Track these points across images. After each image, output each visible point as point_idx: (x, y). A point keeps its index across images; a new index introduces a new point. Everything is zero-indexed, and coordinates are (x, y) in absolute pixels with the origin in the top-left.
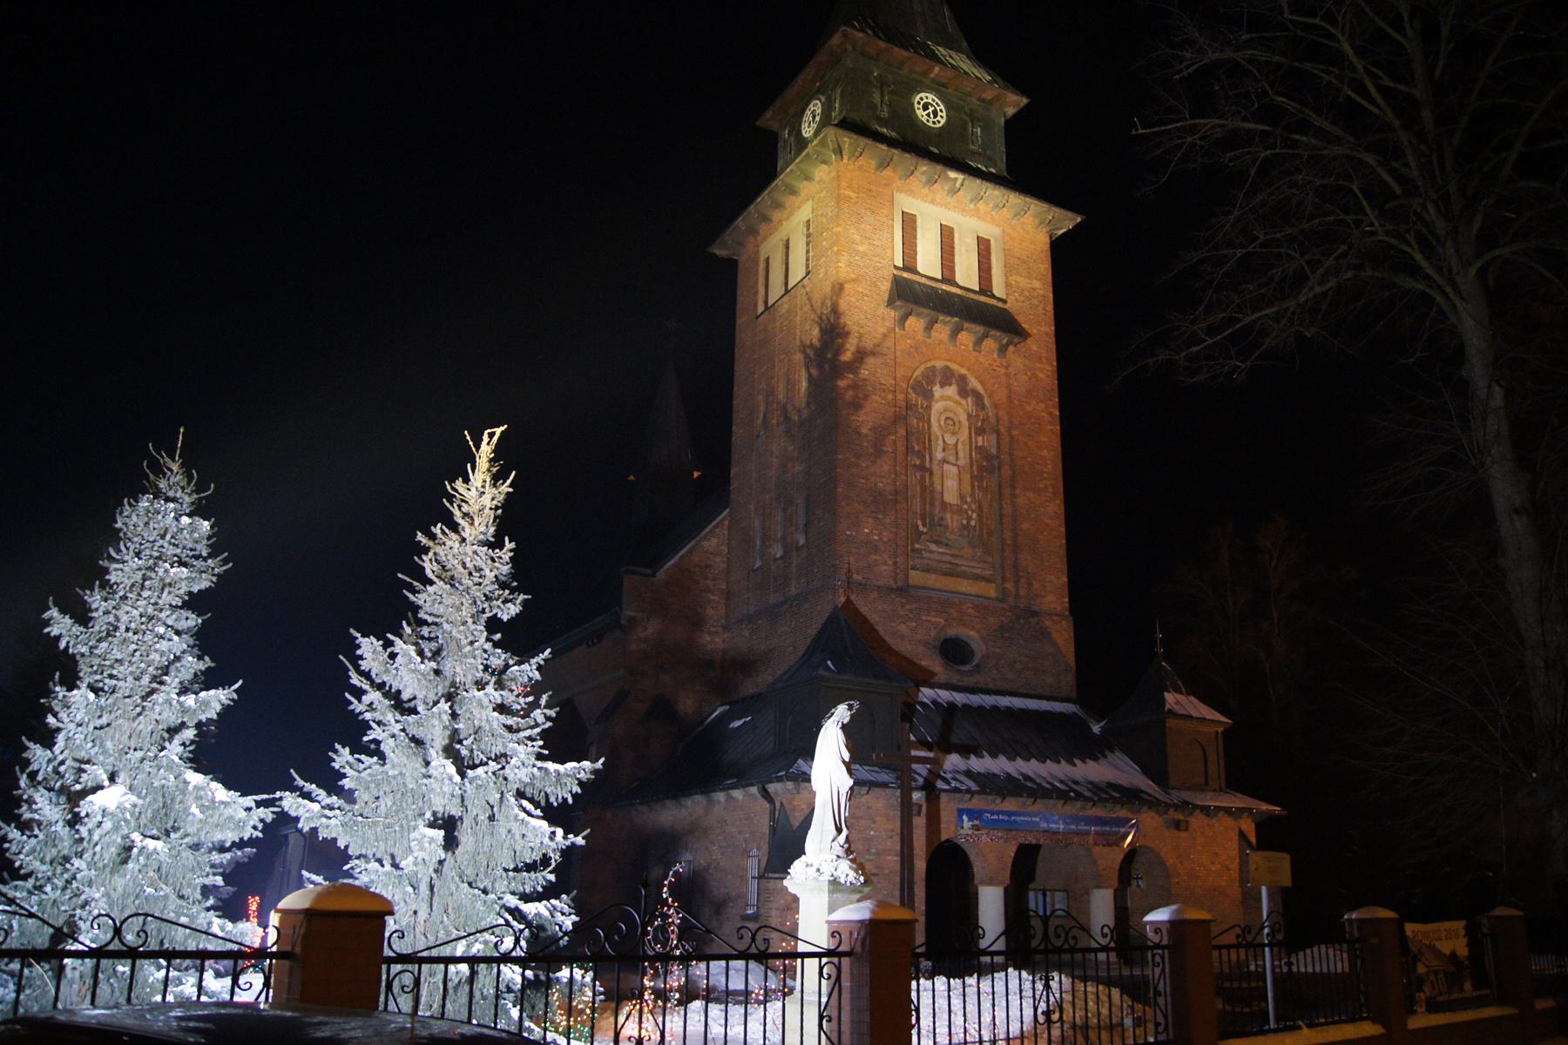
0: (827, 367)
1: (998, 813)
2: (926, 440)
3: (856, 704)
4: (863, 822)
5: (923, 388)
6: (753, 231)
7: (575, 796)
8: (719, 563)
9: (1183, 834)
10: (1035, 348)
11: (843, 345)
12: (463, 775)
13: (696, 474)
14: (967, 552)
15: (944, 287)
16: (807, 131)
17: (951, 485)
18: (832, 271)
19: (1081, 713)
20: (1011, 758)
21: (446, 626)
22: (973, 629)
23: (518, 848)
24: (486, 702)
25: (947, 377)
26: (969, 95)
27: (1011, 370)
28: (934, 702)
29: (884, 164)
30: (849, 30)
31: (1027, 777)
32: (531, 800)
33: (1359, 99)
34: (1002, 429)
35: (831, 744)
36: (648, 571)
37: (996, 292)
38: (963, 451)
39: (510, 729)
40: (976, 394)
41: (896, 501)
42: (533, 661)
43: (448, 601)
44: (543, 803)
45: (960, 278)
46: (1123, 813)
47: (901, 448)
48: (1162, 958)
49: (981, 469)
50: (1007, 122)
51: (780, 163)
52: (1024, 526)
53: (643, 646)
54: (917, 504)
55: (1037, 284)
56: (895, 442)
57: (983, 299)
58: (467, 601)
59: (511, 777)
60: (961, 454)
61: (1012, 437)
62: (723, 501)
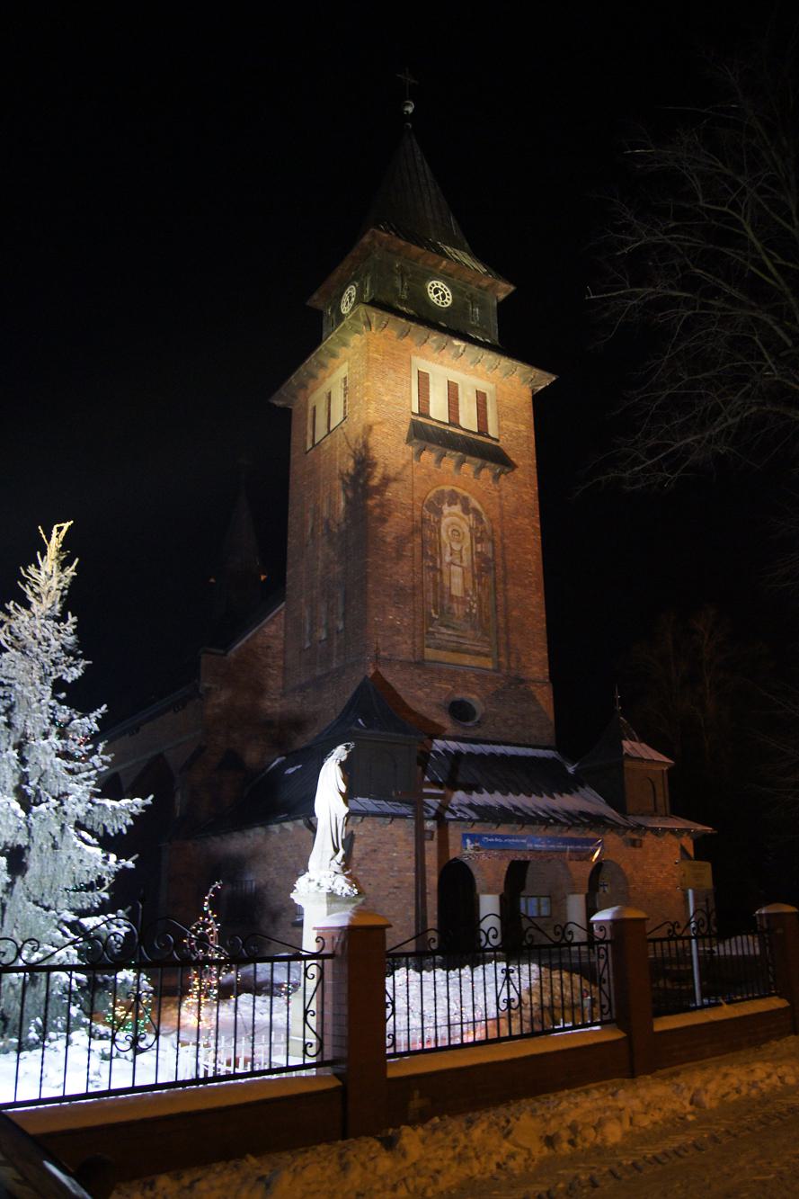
0: (360, 490)
1: (494, 836)
2: (437, 546)
3: (352, 745)
4: (387, 847)
5: (435, 507)
6: (303, 386)
7: (129, 827)
8: (277, 645)
9: (638, 850)
10: (521, 476)
11: (371, 473)
12: (28, 811)
13: (263, 577)
14: (470, 633)
15: (451, 429)
16: (345, 309)
17: (457, 582)
18: (363, 415)
19: (559, 758)
20: (505, 794)
21: (18, 687)
22: (474, 693)
23: (77, 872)
24: (49, 749)
25: (453, 498)
26: (470, 283)
27: (503, 493)
28: (445, 751)
29: (403, 334)
30: (376, 231)
31: (517, 809)
32: (91, 832)
33: (759, 273)
34: (496, 539)
35: (330, 779)
36: (222, 652)
37: (491, 433)
38: (466, 557)
39: (71, 772)
40: (475, 511)
41: (414, 595)
42: (92, 715)
43: (21, 665)
44: (101, 833)
45: (462, 423)
46: (591, 835)
47: (417, 553)
48: (606, 950)
49: (480, 569)
50: (498, 304)
51: (324, 334)
52: (514, 613)
53: (217, 710)
54: (430, 597)
55: (522, 428)
56: (413, 548)
57: (480, 438)
58: (36, 666)
59: (69, 812)
60: (464, 558)
61: (504, 547)
62: (282, 598)
